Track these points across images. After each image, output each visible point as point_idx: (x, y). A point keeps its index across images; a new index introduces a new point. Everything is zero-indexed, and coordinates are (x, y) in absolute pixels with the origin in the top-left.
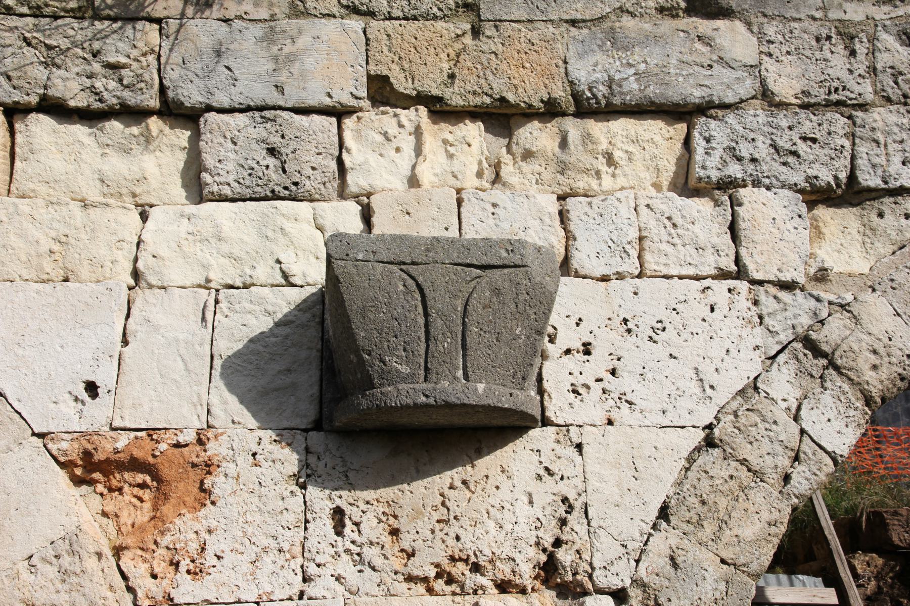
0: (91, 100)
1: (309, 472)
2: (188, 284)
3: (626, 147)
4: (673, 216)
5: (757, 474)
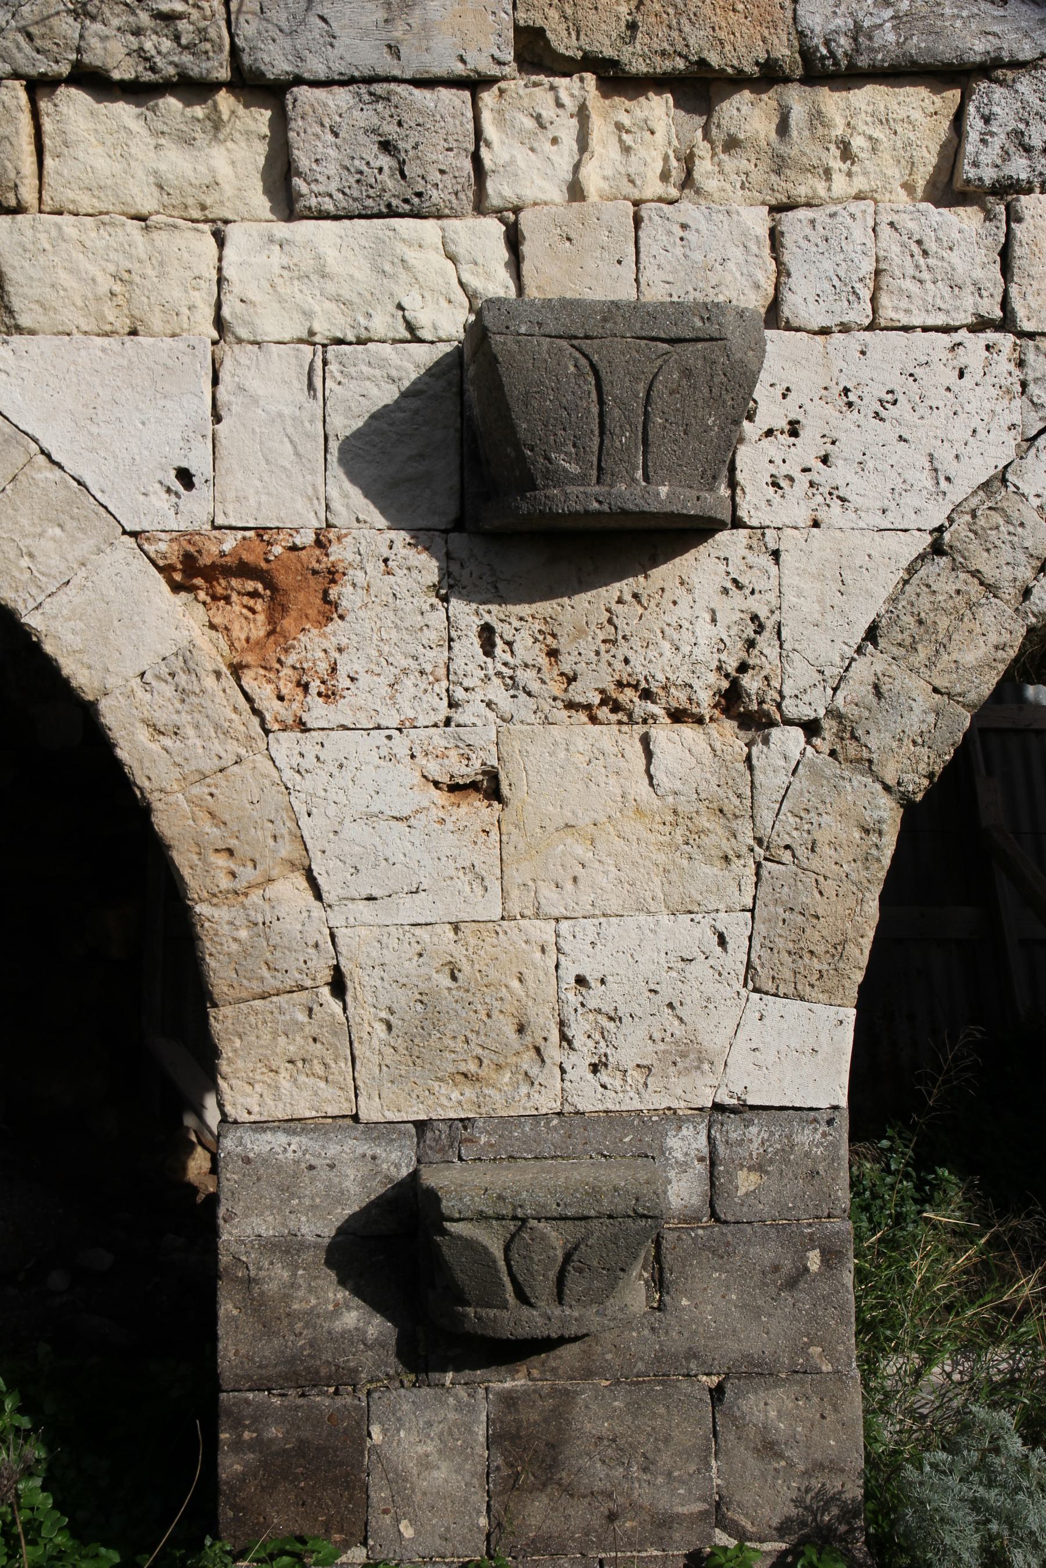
0: (140, 69)
1: (452, 582)
2: (287, 338)
3: (869, 131)
4: (925, 239)
5: (991, 589)
